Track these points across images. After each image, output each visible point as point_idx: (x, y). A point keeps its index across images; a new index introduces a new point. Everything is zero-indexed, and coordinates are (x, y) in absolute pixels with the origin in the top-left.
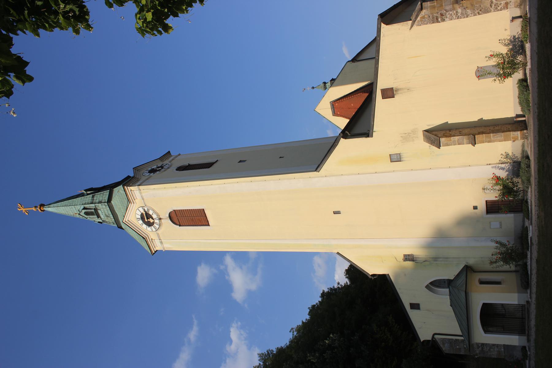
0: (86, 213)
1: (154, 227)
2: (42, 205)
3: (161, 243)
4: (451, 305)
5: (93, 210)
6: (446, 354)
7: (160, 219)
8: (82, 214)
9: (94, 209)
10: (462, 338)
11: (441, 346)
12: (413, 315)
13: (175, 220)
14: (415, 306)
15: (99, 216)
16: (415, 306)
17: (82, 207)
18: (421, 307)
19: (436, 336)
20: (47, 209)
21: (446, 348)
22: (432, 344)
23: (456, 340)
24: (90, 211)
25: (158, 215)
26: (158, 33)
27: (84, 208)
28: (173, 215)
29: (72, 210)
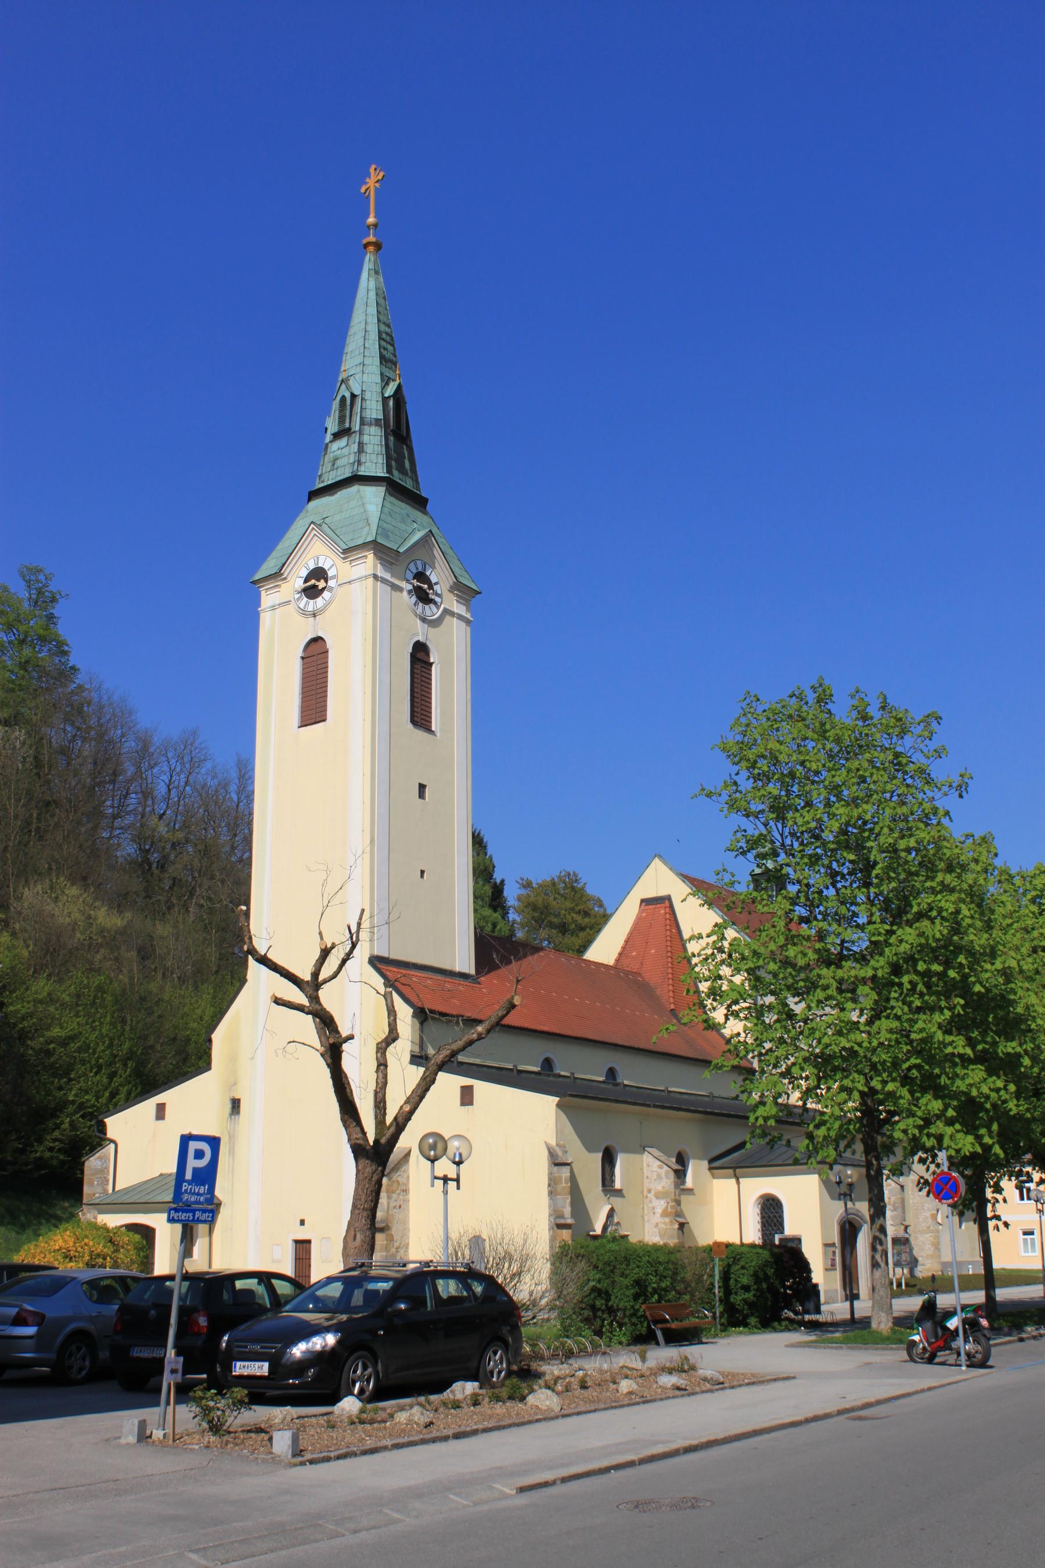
0: (343, 398)
1: (307, 604)
2: (378, 246)
3: (273, 608)
4: (161, 1175)
5: (347, 425)
6: (83, 1163)
7: (314, 615)
8: (344, 392)
9: (350, 429)
10: (110, 1191)
11: (97, 1155)
12: (148, 1106)
13: (313, 646)
14: (161, 1111)
15: (337, 436)
16: (161, 1111)
17: (357, 392)
18: (160, 1122)
19: (112, 1146)
20: (369, 261)
21: (92, 1163)
22: (98, 1139)
23: (108, 1181)
24: (348, 420)
25: (323, 610)
26: (730, 1279)
27: (353, 396)
28: (320, 642)
29: (361, 370)
